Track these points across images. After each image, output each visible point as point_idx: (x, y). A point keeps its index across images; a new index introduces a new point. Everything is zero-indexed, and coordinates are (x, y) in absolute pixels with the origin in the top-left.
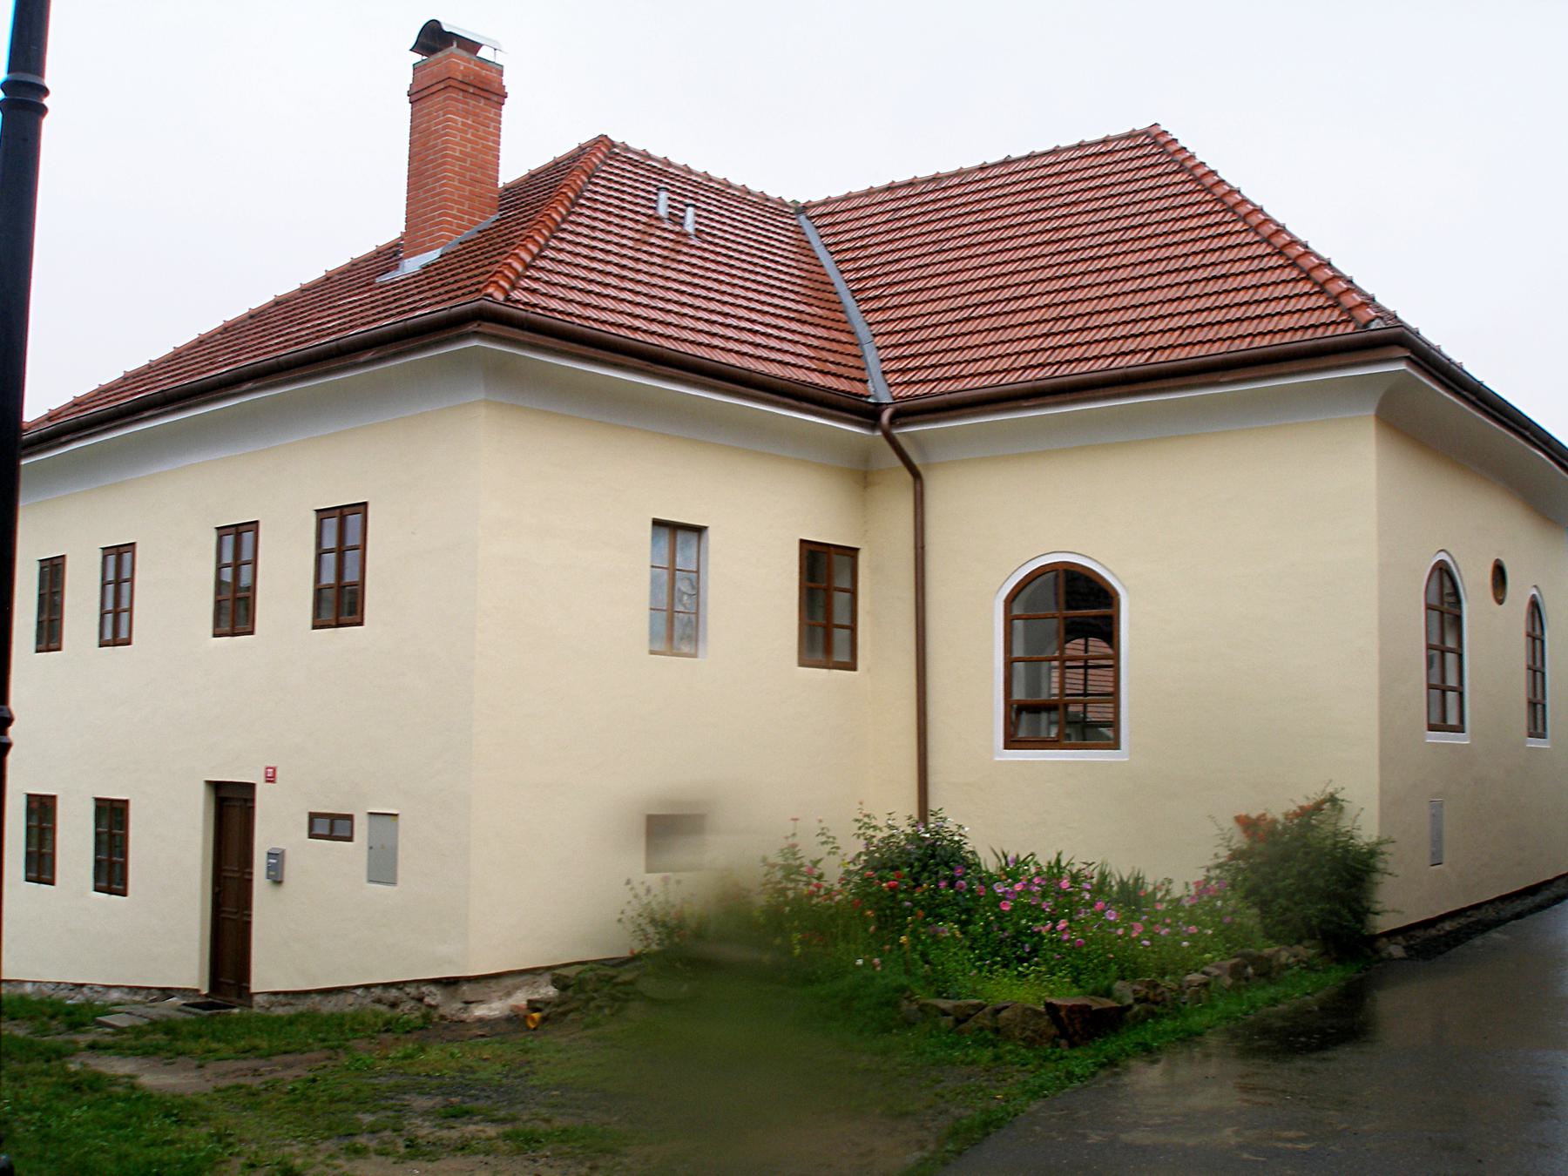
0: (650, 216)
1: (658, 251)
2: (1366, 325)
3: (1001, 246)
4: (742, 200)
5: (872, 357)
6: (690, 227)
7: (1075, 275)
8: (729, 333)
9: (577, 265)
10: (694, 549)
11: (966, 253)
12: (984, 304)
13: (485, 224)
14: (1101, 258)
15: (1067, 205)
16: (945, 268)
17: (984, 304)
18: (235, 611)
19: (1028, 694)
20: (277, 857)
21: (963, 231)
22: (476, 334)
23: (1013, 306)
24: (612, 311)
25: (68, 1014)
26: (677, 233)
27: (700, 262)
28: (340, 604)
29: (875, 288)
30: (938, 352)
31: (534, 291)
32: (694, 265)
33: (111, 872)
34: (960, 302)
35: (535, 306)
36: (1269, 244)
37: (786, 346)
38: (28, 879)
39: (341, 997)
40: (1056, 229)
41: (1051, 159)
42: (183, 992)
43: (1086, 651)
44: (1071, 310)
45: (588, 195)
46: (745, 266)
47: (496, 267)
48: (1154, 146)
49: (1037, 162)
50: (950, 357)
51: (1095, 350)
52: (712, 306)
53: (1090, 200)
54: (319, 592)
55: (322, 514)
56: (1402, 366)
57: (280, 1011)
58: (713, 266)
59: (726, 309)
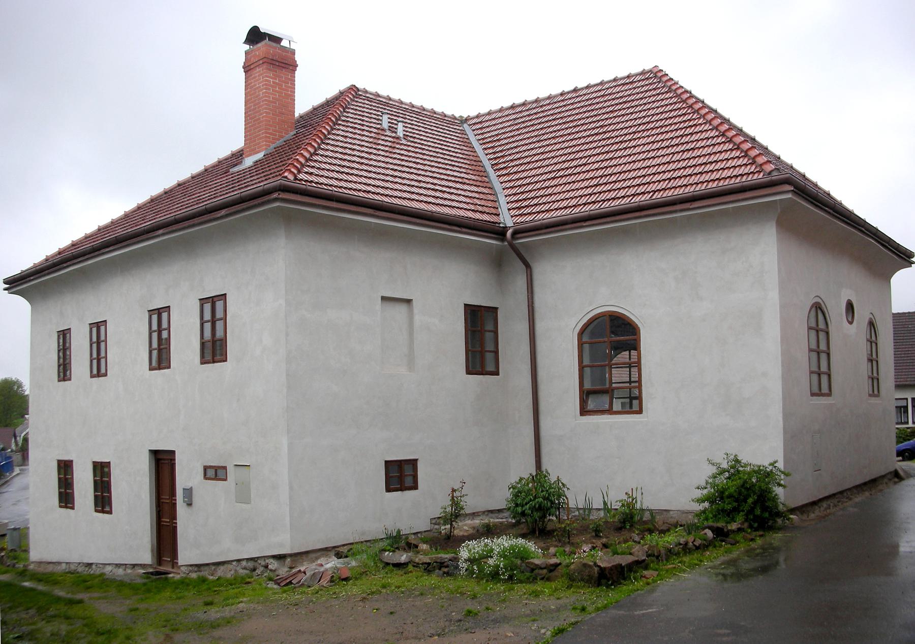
0: (378, 129)
1: (382, 148)
2: (770, 173)
3: (572, 137)
4: (430, 117)
5: (502, 200)
6: (400, 133)
7: (612, 151)
8: (421, 191)
9: (335, 158)
10: (521, 282)
11: (553, 141)
12: (563, 169)
13: (287, 137)
14: (626, 141)
15: (607, 113)
16: (542, 150)
17: (563, 169)
18: (161, 357)
19: (592, 385)
20: (188, 492)
21: (551, 129)
22: (276, 200)
23: (578, 170)
24: (355, 182)
25: (88, 579)
26: (393, 137)
27: (406, 153)
28: (214, 350)
29: (504, 162)
30: (538, 197)
31: (311, 174)
32: (402, 155)
33: (103, 502)
34: (550, 169)
35: (312, 182)
36: (717, 130)
37: (453, 197)
38: (61, 507)
39: (226, 565)
40: (602, 127)
41: (599, 88)
42: (143, 566)
43: (630, 359)
44: (609, 171)
45: (343, 118)
46: (431, 153)
47: (290, 162)
48: (655, 78)
49: (592, 90)
50: (544, 200)
51: (622, 193)
52: (412, 177)
53: (620, 110)
54: (203, 345)
55: (203, 301)
56: (790, 196)
57: (194, 576)
58: (413, 155)
59: (420, 178)
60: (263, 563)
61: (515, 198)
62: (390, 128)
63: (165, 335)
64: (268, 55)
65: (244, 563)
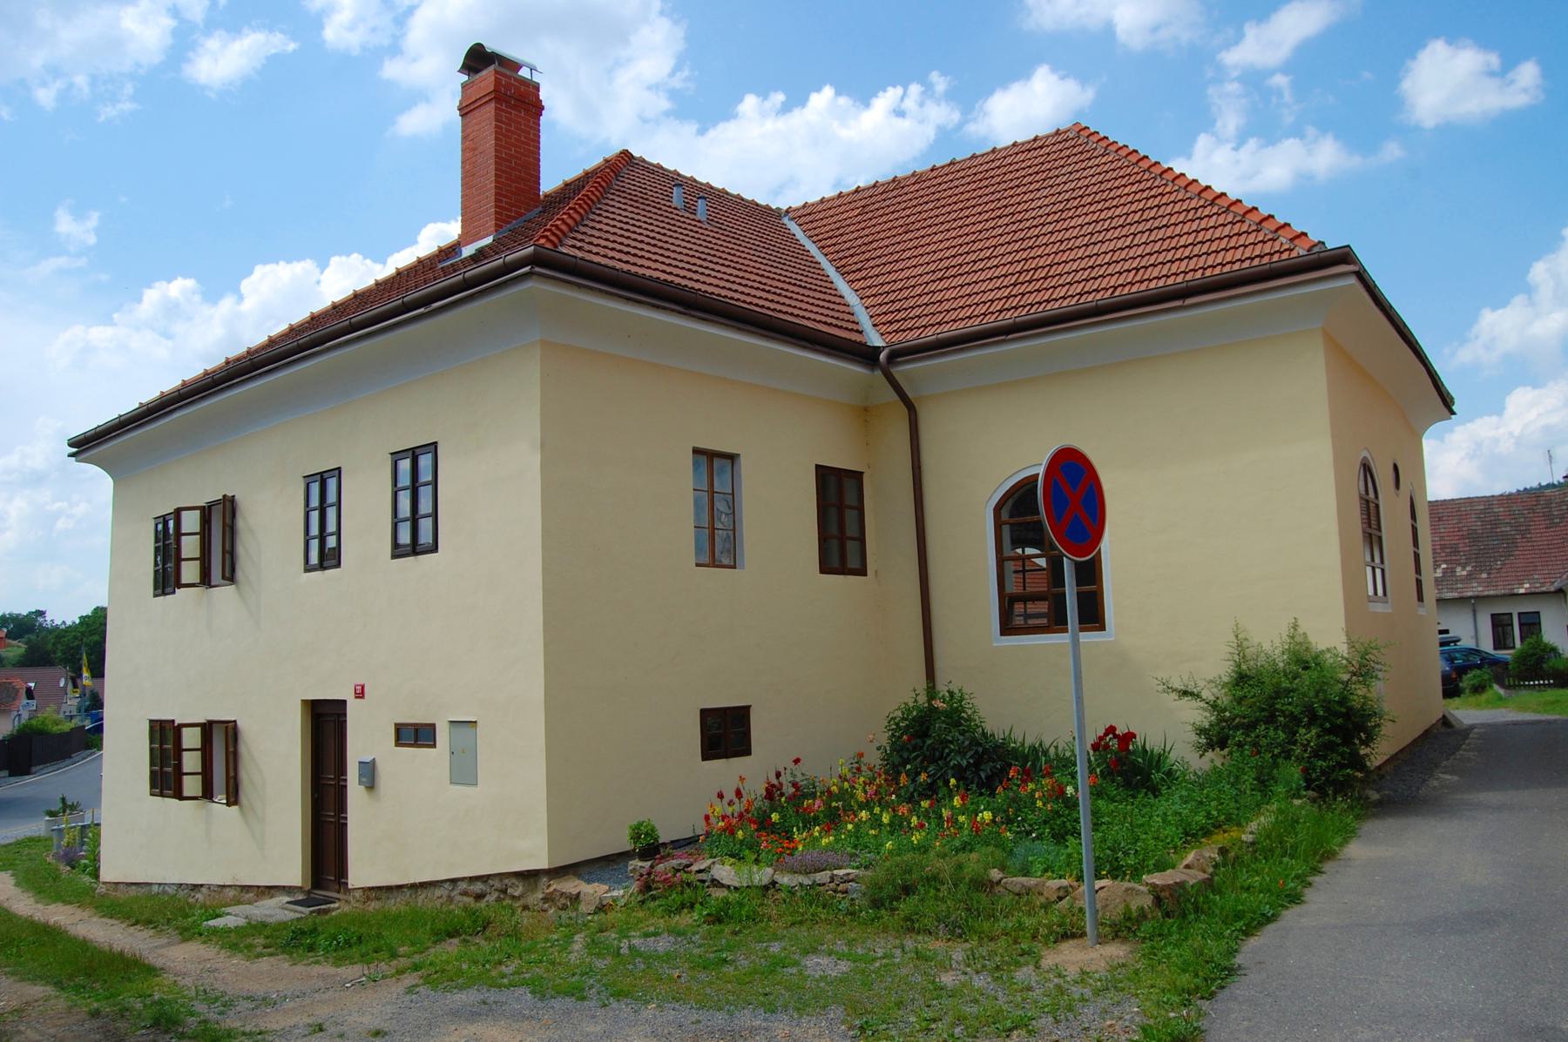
20: (369, 773)
28: (414, 540)
55: (396, 456)
60: (497, 885)
61: (884, 309)
62: (686, 209)
63: (331, 542)
64: (502, 97)
65: (463, 886)
